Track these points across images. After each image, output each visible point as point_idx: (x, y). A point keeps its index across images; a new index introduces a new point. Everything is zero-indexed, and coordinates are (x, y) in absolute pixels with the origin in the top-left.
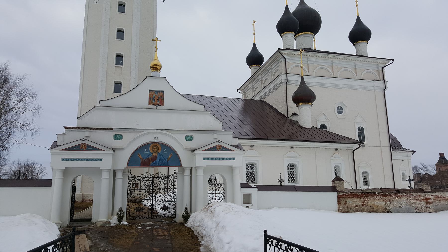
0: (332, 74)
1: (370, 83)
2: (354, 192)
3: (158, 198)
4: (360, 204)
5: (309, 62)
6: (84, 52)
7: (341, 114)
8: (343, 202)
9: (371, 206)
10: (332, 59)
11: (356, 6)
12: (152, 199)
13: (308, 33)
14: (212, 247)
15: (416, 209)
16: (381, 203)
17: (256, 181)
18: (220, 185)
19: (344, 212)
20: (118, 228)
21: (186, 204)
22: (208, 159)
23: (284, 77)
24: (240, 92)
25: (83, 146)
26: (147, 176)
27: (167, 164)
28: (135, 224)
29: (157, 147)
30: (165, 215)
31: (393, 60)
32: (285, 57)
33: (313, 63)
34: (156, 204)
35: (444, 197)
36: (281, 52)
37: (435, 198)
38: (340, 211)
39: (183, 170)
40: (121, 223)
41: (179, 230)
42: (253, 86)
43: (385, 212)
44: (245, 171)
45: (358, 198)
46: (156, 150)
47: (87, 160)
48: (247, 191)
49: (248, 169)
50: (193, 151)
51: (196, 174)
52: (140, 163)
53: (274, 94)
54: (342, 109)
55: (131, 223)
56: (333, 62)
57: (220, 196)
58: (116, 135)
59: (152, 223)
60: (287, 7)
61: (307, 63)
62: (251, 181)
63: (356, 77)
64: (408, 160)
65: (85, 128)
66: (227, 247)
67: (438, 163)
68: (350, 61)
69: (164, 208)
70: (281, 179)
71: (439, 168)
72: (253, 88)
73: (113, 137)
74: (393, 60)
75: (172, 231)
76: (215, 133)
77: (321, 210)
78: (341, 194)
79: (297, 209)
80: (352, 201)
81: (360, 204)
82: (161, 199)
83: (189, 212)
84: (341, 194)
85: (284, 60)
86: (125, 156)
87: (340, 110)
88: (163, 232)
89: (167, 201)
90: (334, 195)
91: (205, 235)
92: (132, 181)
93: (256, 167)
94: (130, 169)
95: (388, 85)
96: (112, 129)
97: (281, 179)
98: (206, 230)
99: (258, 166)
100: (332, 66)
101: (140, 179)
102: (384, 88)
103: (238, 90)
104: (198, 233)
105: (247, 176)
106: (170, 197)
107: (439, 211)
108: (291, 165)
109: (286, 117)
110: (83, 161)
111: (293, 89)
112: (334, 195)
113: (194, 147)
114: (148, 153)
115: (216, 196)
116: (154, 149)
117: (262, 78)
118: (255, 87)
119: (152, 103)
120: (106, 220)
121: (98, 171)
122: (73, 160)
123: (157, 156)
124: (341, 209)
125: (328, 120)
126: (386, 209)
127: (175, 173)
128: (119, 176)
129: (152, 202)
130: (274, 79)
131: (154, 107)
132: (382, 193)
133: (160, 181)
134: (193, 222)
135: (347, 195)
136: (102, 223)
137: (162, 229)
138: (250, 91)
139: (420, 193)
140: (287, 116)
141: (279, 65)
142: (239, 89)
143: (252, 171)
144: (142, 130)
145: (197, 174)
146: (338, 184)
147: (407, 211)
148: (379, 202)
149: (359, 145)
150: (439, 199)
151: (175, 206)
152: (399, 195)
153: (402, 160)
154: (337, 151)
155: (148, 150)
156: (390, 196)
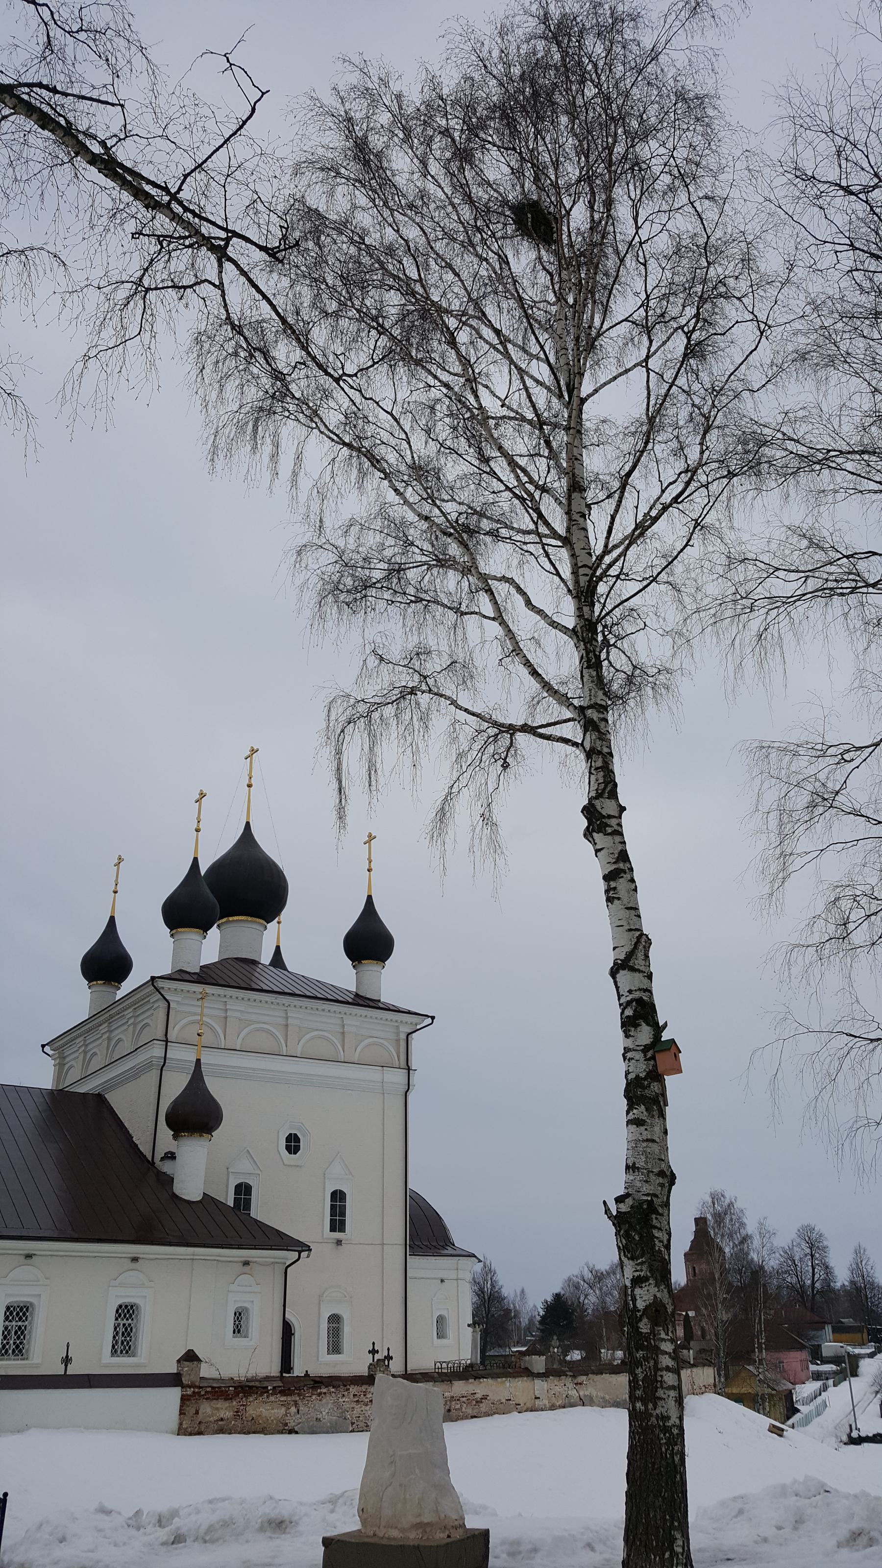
0: (284, 1045)
1: (373, 1075)
2: (219, 1388)
4: (228, 1414)
7: (295, 1153)
11: (369, 870)
13: (250, 919)
15: (353, 1424)
17: (27, 1351)
19: (190, 1434)
23: (157, 1051)
24: (51, 1053)
31: (433, 1018)
33: (237, 1014)
36: (160, 984)
38: (182, 1431)
42: (87, 1045)
43: (282, 1433)
45: (226, 1399)
60: (195, 860)
62: (14, 1351)
67: (690, 1249)
70: (67, 1356)
71: (694, 1268)
72: (85, 1052)
74: (433, 1018)
78: (189, 1391)
81: (228, 1414)
84: (189, 1391)
87: (293, 1144)
90: (174, 1395)
93: (32, 1314)
95: (415, 1078)
97: (67, 1356)
100: (287, 1025)
103: (43, 1046)
105: (5, 1338)
108: (126, 1306)
109: (148, 1161)
112: (174, 1395)
117: (112, 1031)
118: (90, 1050)
124: (184, 1426)
125: (259, 1172)
126: (286, 1424)
135: (203, 1393)
138: (78, 1057)
139: (367, 1386)
140: (150, 1159)
143: (20, 1323)
146: (187, 1367)
147: (334, 1429)
148: (273, 1409)
153: (442, 1281)
154: (247, 1268)
156: (299, 1395)
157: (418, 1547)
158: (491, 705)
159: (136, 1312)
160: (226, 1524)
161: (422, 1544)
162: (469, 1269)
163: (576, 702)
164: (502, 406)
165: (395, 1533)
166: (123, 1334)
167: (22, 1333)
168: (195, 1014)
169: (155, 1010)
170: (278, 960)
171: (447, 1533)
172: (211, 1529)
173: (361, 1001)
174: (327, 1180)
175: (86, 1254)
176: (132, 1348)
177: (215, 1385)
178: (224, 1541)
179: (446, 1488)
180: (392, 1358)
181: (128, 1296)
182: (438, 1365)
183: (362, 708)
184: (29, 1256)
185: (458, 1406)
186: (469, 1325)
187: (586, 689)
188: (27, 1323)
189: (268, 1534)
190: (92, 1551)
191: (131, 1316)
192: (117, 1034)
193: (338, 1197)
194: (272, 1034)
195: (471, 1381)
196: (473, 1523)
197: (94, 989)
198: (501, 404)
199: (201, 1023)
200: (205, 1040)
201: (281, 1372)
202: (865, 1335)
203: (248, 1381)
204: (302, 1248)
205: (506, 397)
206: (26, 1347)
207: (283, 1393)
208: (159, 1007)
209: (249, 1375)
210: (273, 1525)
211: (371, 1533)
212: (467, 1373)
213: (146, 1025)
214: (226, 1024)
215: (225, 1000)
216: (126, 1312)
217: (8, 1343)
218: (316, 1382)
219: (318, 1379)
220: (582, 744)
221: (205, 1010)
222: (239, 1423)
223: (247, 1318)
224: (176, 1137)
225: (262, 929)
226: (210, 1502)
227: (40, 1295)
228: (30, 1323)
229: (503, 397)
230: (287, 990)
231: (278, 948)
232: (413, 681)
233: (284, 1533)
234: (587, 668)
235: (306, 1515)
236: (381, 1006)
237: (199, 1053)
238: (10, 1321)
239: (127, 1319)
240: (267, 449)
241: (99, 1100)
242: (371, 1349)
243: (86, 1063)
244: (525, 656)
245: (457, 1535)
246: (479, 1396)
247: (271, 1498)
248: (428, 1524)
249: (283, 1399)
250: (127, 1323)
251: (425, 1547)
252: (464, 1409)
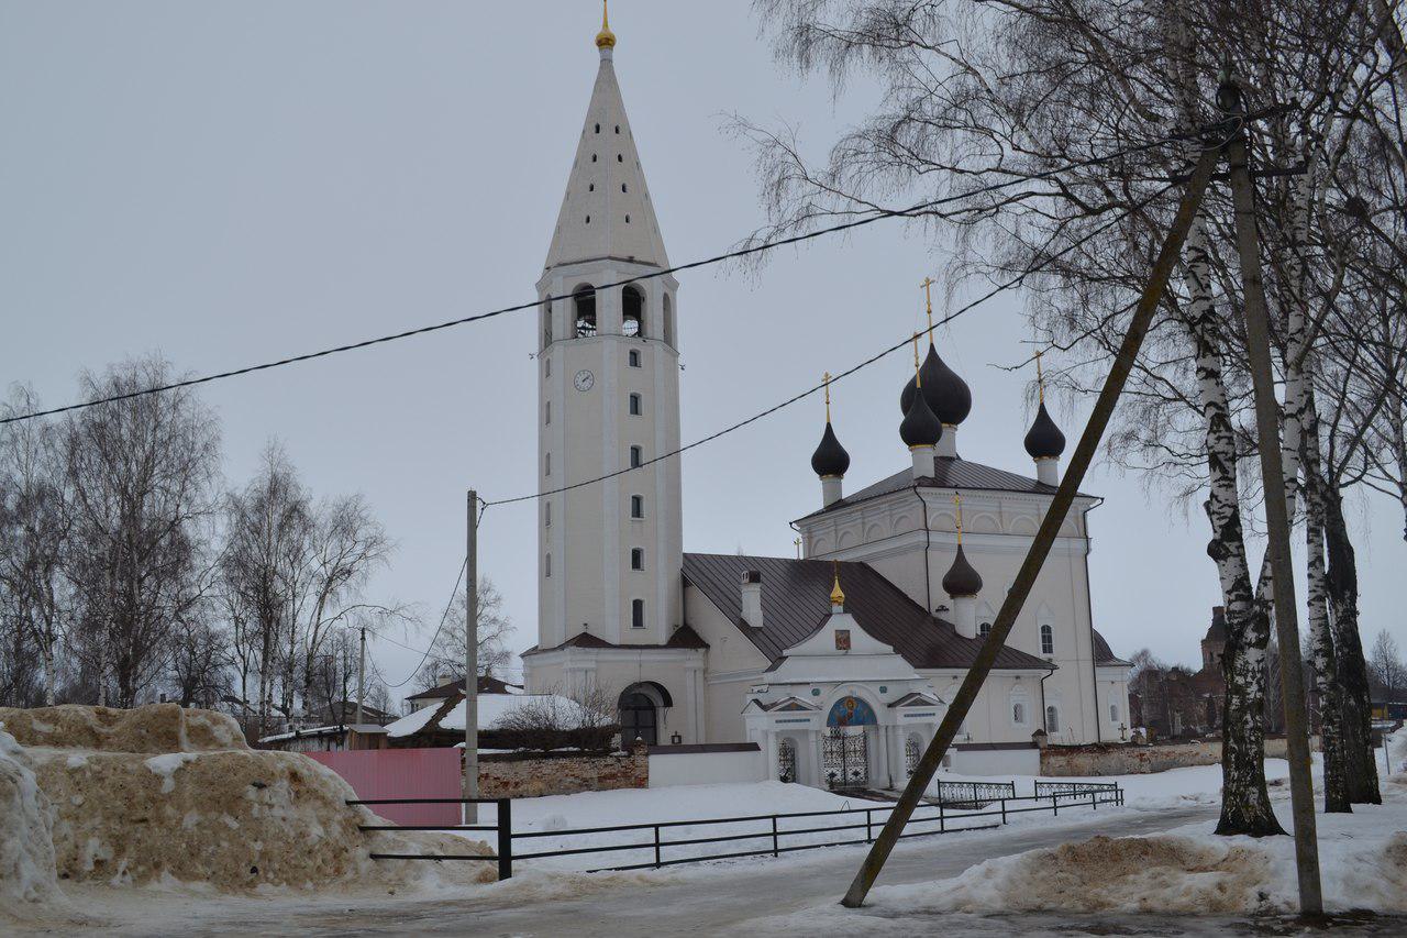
8: (1046, 761)
31: (1102, 499)
67: (1208, 636)
69: (856, 774)
74: (1102, 499)
96: (808, 684)
103: (791, 524)
112: (1036, 753)
121: (805, 732)
131: (843, 651)
146: (1040, 738)
193: (1046, 630)
194: (991, 519)
202: (1386, 711)
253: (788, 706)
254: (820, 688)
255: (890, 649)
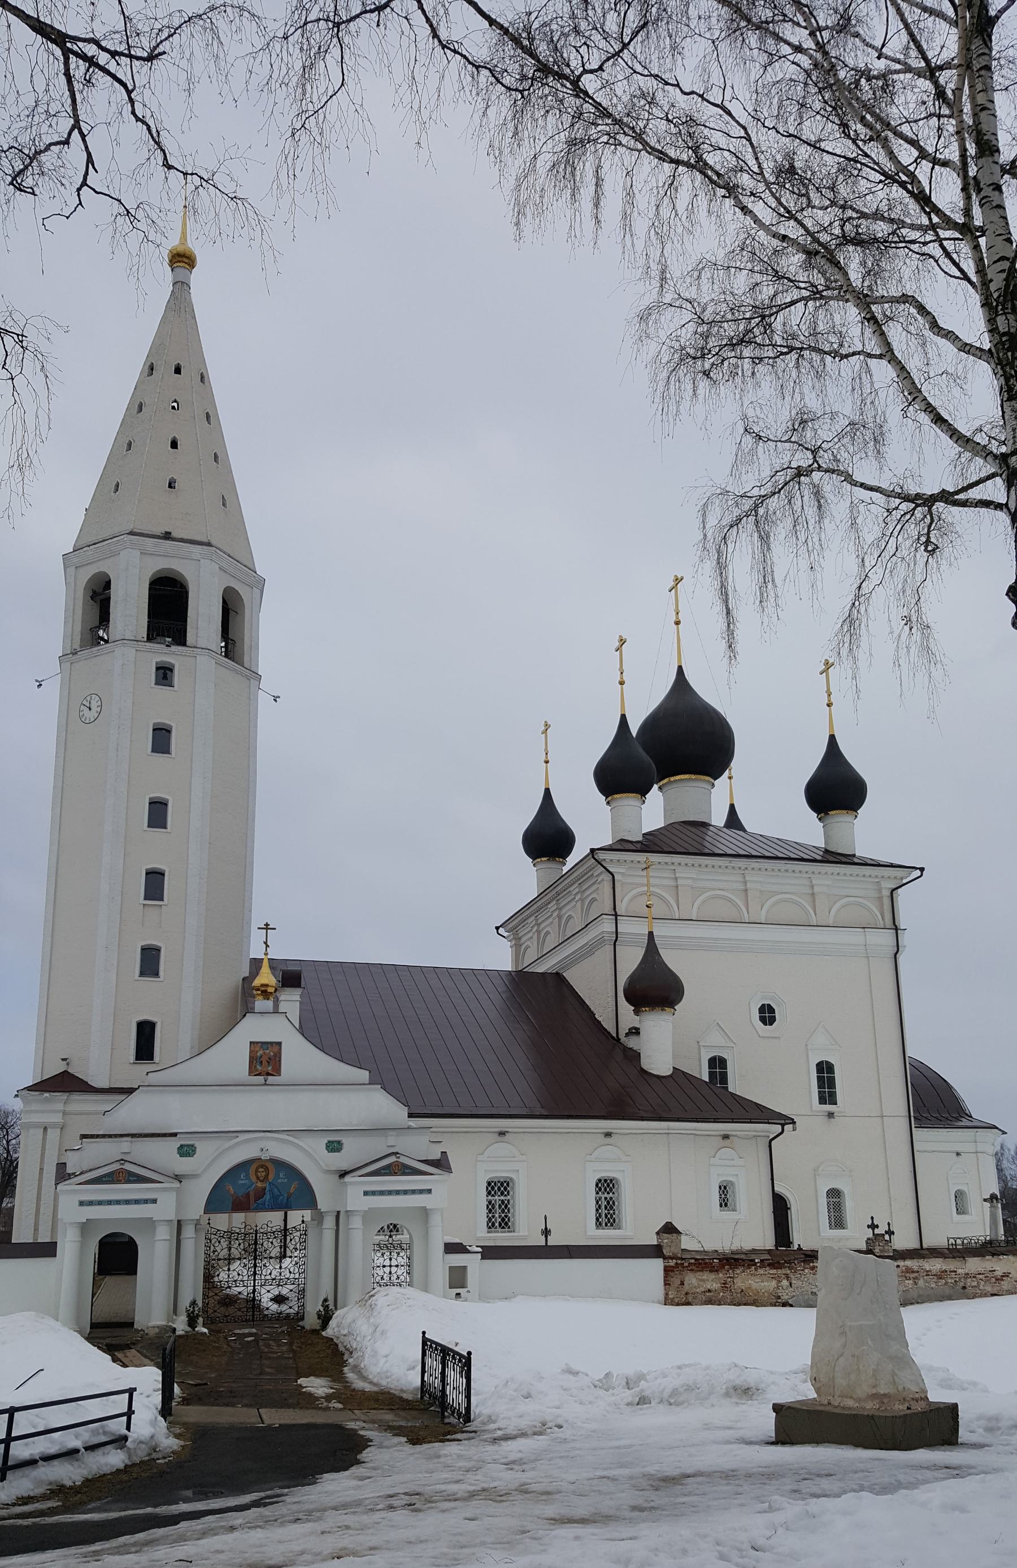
1: (856, 937)
2: (703, 1259)
3: (267, 1277)
4: (716, 1286)
5: (680, 882)
6: (55, 860)
7: (771, 1024)
8: (676, 1281)
9: (742, 1291)
10: (746, 871)
11: (828, 705)
12: (255, 1280)
13: (693, 777)
14: (362, 1366)
16: (766, 1283)
17: (513, 1224)
18: (401, 1247)
19: (678, 1304)
20: (190, 1339)
21: (326, 1289)
22: (374, 1193)
24: (506, 934)
25: (121, 1174)
26: (243, 1231)
27: (285, 1206)
28: (219, 1332)
29: (267, 1169)
30: (281, 1313)
31: (922, 870)
32: (611, 870)
33: (690, 882)
34: (263, 1291)
35: (928, 1271)
36: (601, 856)
37: (902, 1272)
38: (668, 1301)
39: (319, 1217)
40: (194, 1330)
41: (309, 1342)
43: (775, 1306)
44: (482, 1199)
45: (711, 1271)
46: (264, 1174)
47: (127, 1202)
48: (457, 1260)
49: (493, 1193)
50: (343, 1174)
51: (348, 1225)
52: (231, 1205)
53: (586, 964)
54: (771, 1010)
55: (213, 1331)
56: (747, 878)
57: (399, 1273)
58: (182, 1146)
59: (254, 1330)
60: (623, 718)
61: (673, 883)
62: (500, 1224)
63: (814, 920)
64: (977, 1152)
65: (122, 1136)
66: (382, 1361)
68: (796, 875)
69: (279, 1299)
70: (546, 1228)
72: (539, 932)
73: (176, 1151)
74: (922, 870)
75: (296, 1344)
76: (391, 1133)
77: (624, 1299)
78: (672, 1263)
79: (570, 1298)
80: (697, 1279)
81: (716, 1286)
82: (273, 1279)
83: (331, 1307)
84: (672, 1263)
85: (607, 877)
86: (203, 1189)
87: (767, 1015)
88: (279, 1346)
89: (286, 1284)
90: (657, 1266)
91: (356, 1349)
92: (213, 1242)
94: (212, 1216)
95: (905, 939)
96: (175, 1135)
97: (546, 1228)
98: (358, 1339)
99: (517, 1185)
100: (746, 890)
101: (230, 1238)
102: (896, 949)
103: (497, 928)
104: (345, 1347)
105: (490, 1211)
106: (292, 1276)
107: (912, 1304)
108: (606, 1181)
109: (613, 1037)
110: (120, 1204)
111: (631, 959)
112: (657, 1266)
113: (345, 1166)
114: (247, 1181)
115: (390, 1273)
116: (259, 1174)
119: (257, 1070)
120: (164, 1323)
122: (100, 1203)
123: (265, 1189)
126: (779, 1297)
127: (303, 1222)
128: (188, 1232)
129: (254, 1286)
130: (586, 926)
131: (260, 1079)
132: (769, 1260)
133: (271, 1240)
134: (338, 1326)
135: (686, 1264)
136: (157, 1330)
137: (277, 1341)
140: (615, 1035)
141: (598, 889)
142: (501, 926)
143: (502, 1198)
144: (236, 1134)
145: (350, 1227)
146: (666, 1239)
148: (763, 1282)
149: (783, 1125)
150: (914, 1275)
151: (302, 1293)
152: (811, 1264)
153: (958, 1154)
154: (727, 1142)
155: (247, 1177)
157: (873, 1416)
158: (900, 472)
159: (616, 1186)
160: (689, 1389)
161: (877, 1414)
162: (990, 1142)
163: (994, 447)
164: (879, 58)
165: (850, 1403)
166: (606, 1208)
167: (506, 1206)
168: (643, 885)
169: (599, 883)
170: (733, 821)
171: (906, 1405)
172: (674, 1392)
173: (832, 857)
174: (810, 1052)
175: (540, 1130)
176: (617, 1220)
177: (698, 1257)
178: (689, 1404)
179: (904, 1360)
180: (893, 1233)
181: (609, 1171)
182: (952, 1241)
183: (747, 504)
184: (502, 1134)
185: (975, 1284)
186: (985, 1200)
187: (1009, 429)
188: (509, 1197)
189: (734, 1400)
190: (558, 1408)
191: (611, 1190)
192: (566, 912)
194: (731, 901)
195: (988, 1257)
196: (937, 1395)
197: (539, 866)
198: (877, 55)
199: (650, 894)
200: (655, 912)
201: (776, 1246)
203: (733, 1253)
204: (785, 1121)
205: (883, 46)
206: (512, 1219)
207: (772, 1265)
208: (603, 880)
209: (734, 1248)
210: (739, 1391)
211: (826, 1402)
212: (987, 1249)
213: (594, 900)
214: (678, 894)
215: (673, 867)
216: (606, 1186)
217: (493, 1217)
218: (807, 1256)
219: (810, 1253)
220: (1007, 504)
221: (645, 881)
222: (727, 1294)
223: (733, 1192)
224: (637, 1012)
225: (709, 787)
226: (679, 1368)
227: (737, 1175)
228: (513, 1198)
229: (878, 43)
230: (742, 852)
231: (732, 807)
232: (803, 459)
233: (751, 1400)
234: (1008, 400)
235: (773, 1383)
236: (856, 860)
237: (650, 925)
238: (493, 1196)
239: (608, 1193)
240: (587, 192)
241: (558, 978)
242: (870, 1223)
243: (541, 943)
244: (925, 399)
245: (919, 1407)
246: (999, 1273)
247: (736, 1366)
248: (885, 1395)
249: (772, 1272)
250: (608, 1196)
251: (879, 1417)
252: (981, 1287)
253: (110, 1174)
254: (197, 1145)
255: (364, 1075)
